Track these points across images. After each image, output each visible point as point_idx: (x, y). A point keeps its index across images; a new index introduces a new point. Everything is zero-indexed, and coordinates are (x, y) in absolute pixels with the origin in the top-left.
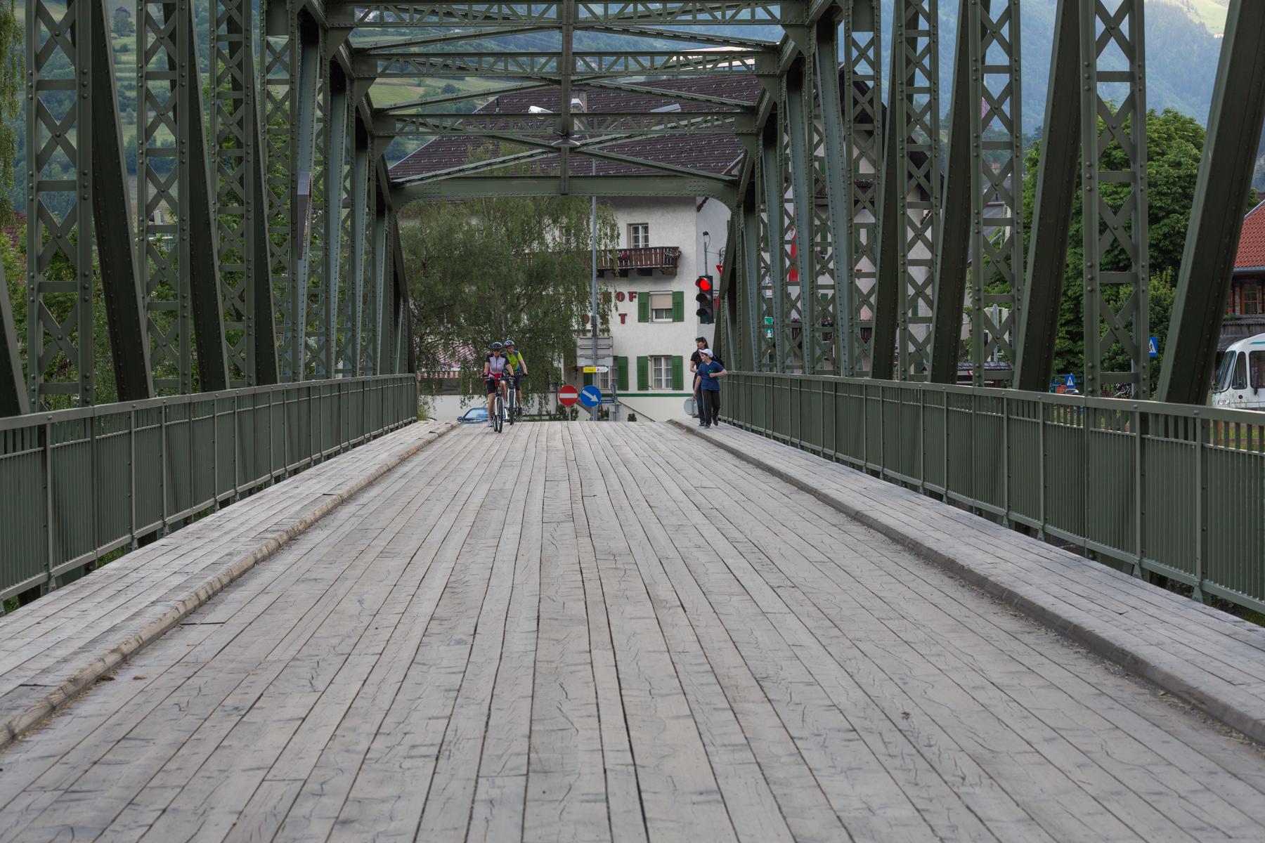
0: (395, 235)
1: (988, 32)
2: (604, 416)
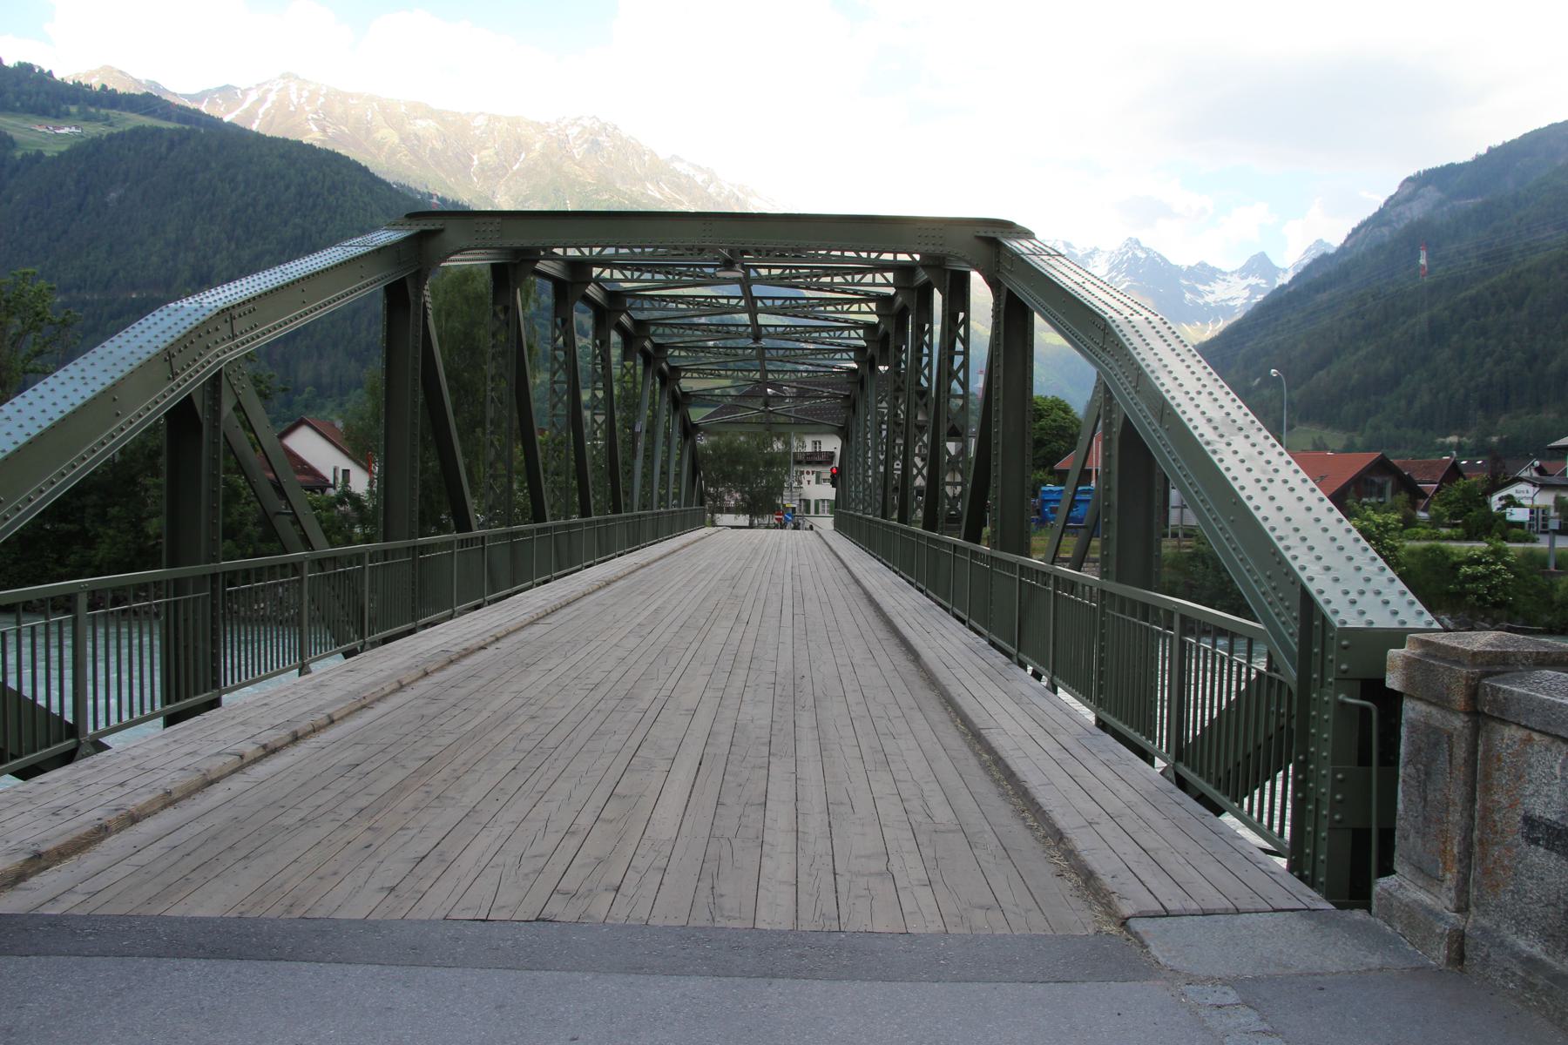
0: (694, 445)
1: (952, 375)
2: (796, 527)
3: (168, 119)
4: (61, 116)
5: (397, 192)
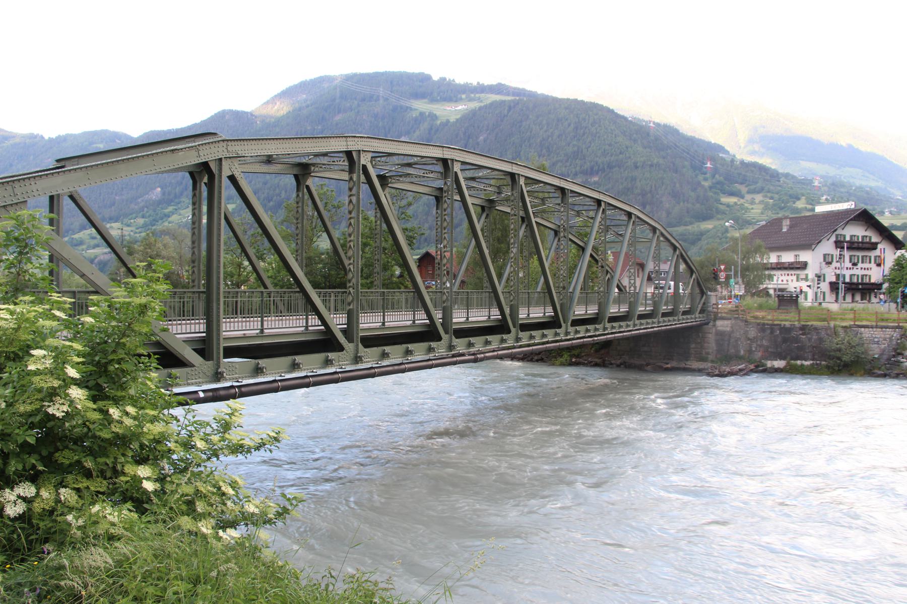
3: (508, 95)
5: (631, 122)
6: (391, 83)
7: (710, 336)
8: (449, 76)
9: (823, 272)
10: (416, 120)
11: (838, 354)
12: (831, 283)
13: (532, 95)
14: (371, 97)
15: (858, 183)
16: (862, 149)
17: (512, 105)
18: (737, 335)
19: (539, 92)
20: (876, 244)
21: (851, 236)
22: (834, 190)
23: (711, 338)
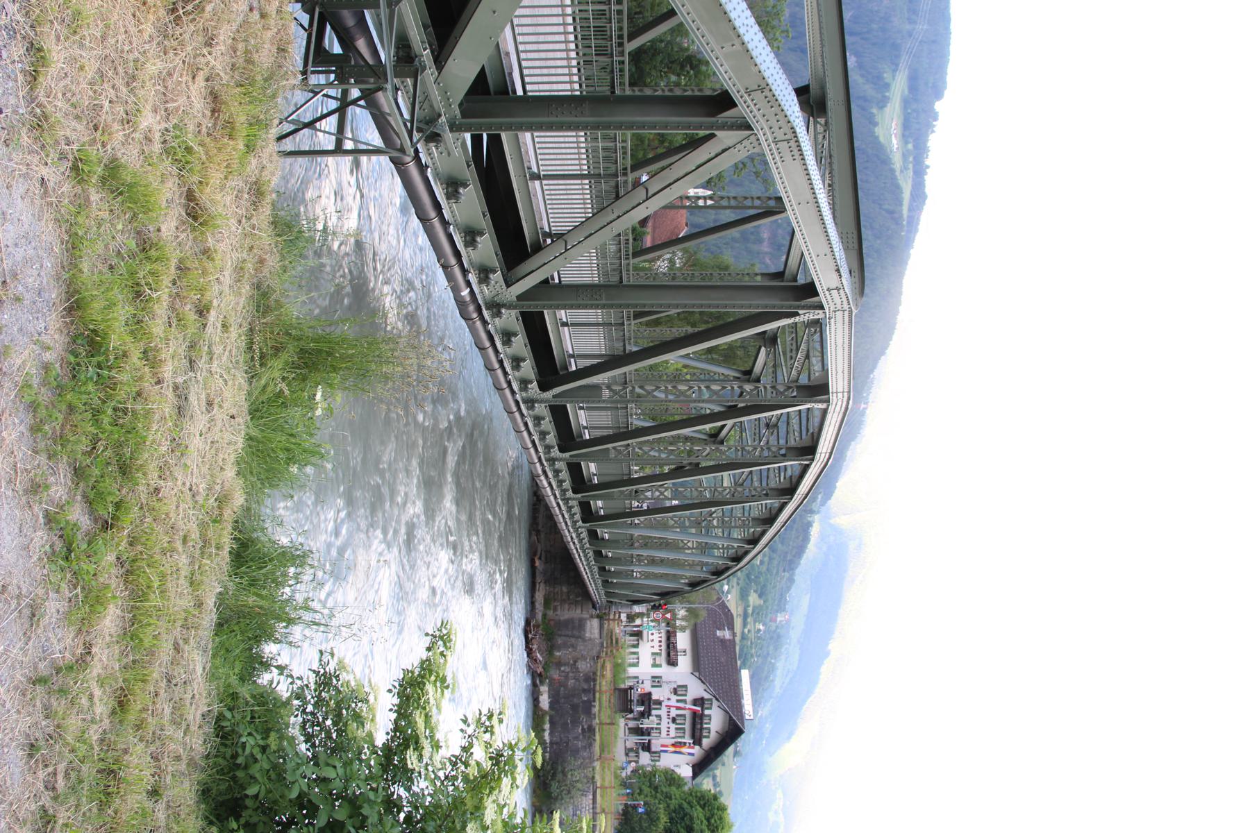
3: (910, 210)
4: (905, 138)
5: (868, 377)
6: (934, 42)
7: (579, 611)
8: (939, 125)
9: (664, 685)
10: (879, 77)
11: (560, 776)
12: (650, 694)
13: (908, 243)
14: (915, 12)
15: (780, 665)
16: (824, 669)
17: (896, 215)
18: (580, 647)
19: (912, 251)
20: (700, 745)
21: (709, 716)
22: (771, 638)
23: (575, 613)
